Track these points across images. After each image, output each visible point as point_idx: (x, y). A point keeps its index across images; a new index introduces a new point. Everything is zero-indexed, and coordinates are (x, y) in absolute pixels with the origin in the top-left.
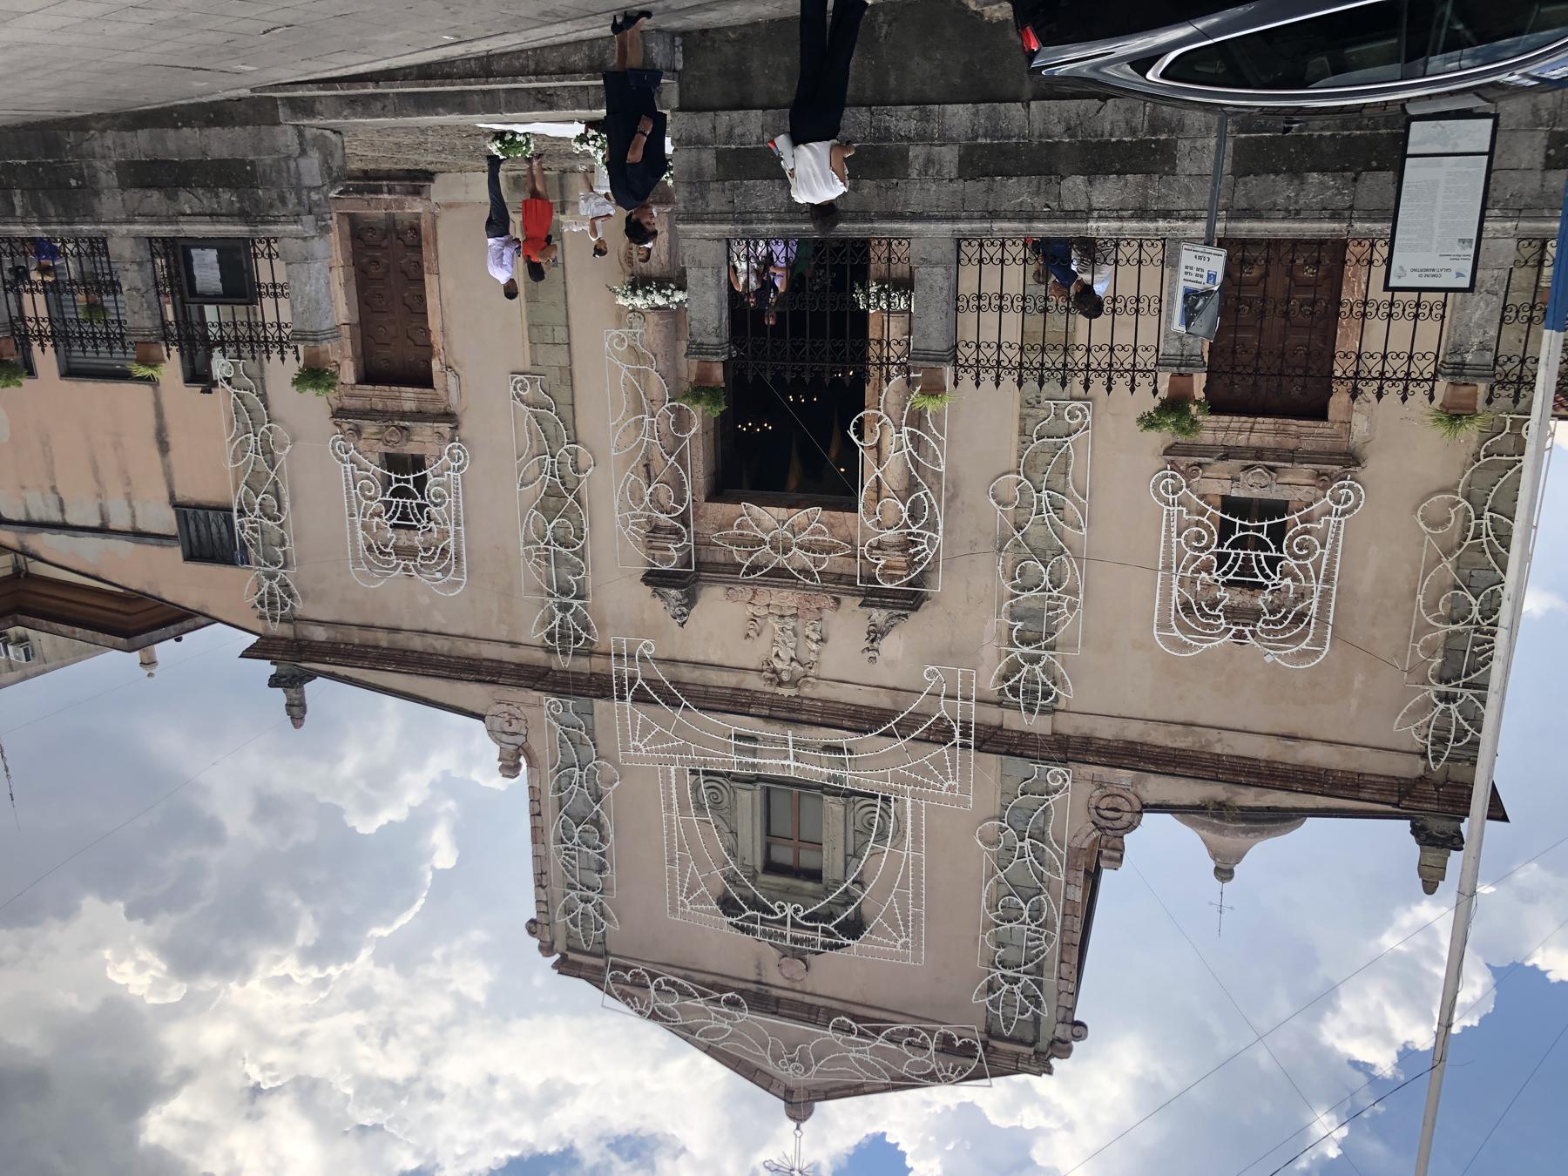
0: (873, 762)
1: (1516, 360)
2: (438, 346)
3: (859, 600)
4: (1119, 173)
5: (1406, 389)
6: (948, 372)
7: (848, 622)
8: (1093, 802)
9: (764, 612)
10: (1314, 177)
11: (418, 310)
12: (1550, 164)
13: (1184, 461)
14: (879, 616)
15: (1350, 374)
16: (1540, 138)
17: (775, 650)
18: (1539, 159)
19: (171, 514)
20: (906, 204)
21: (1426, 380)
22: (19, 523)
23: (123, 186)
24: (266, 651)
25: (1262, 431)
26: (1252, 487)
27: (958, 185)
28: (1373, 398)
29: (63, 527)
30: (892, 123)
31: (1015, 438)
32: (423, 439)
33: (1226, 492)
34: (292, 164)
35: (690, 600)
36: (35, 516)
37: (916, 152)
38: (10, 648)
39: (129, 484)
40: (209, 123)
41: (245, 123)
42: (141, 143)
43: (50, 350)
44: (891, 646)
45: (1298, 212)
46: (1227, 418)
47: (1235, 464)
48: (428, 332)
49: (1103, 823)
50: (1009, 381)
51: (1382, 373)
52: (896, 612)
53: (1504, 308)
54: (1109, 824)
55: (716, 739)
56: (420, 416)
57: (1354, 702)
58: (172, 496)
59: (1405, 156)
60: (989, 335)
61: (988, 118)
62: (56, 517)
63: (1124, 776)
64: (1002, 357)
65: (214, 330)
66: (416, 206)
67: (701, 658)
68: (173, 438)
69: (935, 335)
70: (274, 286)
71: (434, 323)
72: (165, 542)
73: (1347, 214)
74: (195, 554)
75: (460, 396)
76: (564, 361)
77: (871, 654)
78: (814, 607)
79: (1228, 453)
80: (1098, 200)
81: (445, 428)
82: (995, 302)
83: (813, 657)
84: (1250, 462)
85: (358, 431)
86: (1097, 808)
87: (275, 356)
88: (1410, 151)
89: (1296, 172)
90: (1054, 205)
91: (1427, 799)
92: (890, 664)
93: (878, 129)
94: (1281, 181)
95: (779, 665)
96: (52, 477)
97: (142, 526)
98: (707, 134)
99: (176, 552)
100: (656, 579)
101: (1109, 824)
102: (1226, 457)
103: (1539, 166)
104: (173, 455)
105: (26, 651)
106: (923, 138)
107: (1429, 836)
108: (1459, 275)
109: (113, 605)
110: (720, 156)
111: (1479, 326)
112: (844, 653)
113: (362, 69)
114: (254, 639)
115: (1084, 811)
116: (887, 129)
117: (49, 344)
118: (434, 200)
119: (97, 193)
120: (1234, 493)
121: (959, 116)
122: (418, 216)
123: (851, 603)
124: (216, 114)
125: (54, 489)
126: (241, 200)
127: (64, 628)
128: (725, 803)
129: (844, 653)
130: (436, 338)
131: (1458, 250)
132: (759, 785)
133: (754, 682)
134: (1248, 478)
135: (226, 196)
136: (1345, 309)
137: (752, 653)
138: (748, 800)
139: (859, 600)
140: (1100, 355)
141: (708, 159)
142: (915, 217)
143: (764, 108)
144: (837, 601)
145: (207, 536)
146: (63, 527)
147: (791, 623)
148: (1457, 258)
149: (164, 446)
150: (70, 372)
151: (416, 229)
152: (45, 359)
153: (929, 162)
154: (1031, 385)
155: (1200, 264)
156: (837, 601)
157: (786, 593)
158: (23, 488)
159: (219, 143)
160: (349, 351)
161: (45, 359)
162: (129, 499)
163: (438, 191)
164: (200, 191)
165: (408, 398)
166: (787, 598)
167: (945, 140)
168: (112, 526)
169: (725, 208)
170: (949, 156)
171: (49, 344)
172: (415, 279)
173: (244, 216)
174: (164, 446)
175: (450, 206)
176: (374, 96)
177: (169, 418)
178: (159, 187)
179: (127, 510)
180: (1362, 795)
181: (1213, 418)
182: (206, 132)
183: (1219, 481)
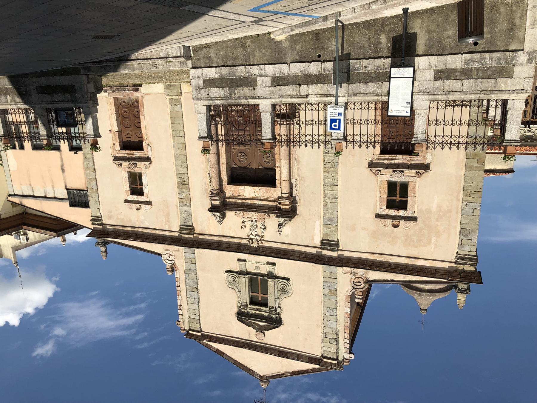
0: (283, 267)
1: (433, 136)
2: (145, 138)
3: (276, 215)
4: (316, 84)
5: (451, 146)
6: (344, 143)
7: (273, 221)
8: (352, 280)
9: (247, 220)
10: (370, 84)
11: (138, 127)
12: (435, 79)
13: (374, 169)
14: (282, 220)
15: (373, 141)
16: (432, 72)
17: (251, 232)
18: (432, 78)
19: (66, 192)
20: (257, 94)
21: (472, 144)
22: (237, 272)
23: (38, 94)
24: (94, 234)
25: (399, 159)
26: (398, 178)
27: (271, 88)
28: (433, 149)
29: (33, 197)
30: (251, 71)
31: (322, 163)
32: (141, 166)
33: (389, 179)
34: (85, 86)
35: (223, 216)
36: (25, 194)
37: (259, 79)
38: (21, 236)
39: (53, 183)
40: (62, 75)
41: (71, 74)
42: (44, 81)
43: (66, 142)
44: (286, 229)
45: (367, 94)
46: (387, 156)
47: (391, 170)
48: (142, 133)
49: (356, 287)
50: (462, 148)
51: (360, 141)
52: (287, 219)
53: (429, 121)
54: (357, 287)
55: (231, 260)
56: (140, 159)
57: (433, 246)
58: (66, 186)
59: (390, 78)
60: (302, 132)
61: (279, 69)
62: (31, 194)
63: (361, 271)
64: (452, 140)
65: (25, 135)
66: (136, 95)
67: (228, 235)
68: (66, 169)
69: (268, 132)
70: (82, 121)
71: (143, 130)
72: (64, 201)
73: (380, 94)
74: (73, 204)
75: (152, 153)
76: (183, 142)
77: (280, 232)
78: (262, 218)
79: (388, 166)
80: (311, 92)
81: (147, 163)
82: (314, 123)
83: (262, 234)
84: (395, 169)
85: (121, 165)
86: (353, 282)
87: (26, 140)
88: (392, 76)
89: (365, 82)
90: (298, 94)
91: (457, 277)
92: (287, 236)
93: (248, 72)
94: (361, 85)
95: (252, 237)
96: (29, 180)
97: (57, 196)
98: (201, 76)
99: (67, 204)
100: (213, 209)
101: (357, 287)
102: (387, 168)
103: (433, 80)
104: (66, 173)
105: (26, 237)
106: (260, 75)
107: (459, 290)
108: (407, 112)
109: (52, 222)
110: (204, 81)
111: (421, 126)
112: (272, 231)
113: (102, 59)
114: (91, 231)
115: (349, 283)
116: (250, 72)
117: (322, 145)
118: (142, 92)
119: (31, 96)
120: (391, 179)
121: (271, 70)
122: (138, 97)
123: (273, 216)
124: (65, 72)
125: (30, 185)
126: (71, 97)
127: (37, 230)
128: (237, 282)
129: (272, 231)
130: (144, 135)
131: (406, 105)
132: (247, 276)
133: (245, 242)
134: (395, 175)
135: (67, 95)
136: (380, 122)
137: (245, 233)
138: (244, 281)
139: (276, 215)
140: (315, 137)
141: (201, 82)
142: (260, 98)
143: (215, 67)
144: (269, 216)
145: (78, 199)
146: (33, 197)
147: (255, 223)
148: (406, 107)
149: (63, 170)
150: (35, 148)
151: (137, 101)
152: (27, 145)
153: (263, 82)
154: (471, 148)
155: (335, 111)
156: (269, 216)
157: (253, 213)
158: (21, 184)
159: (64, 80)
160: (118, 140)
161: (27, 145)
162: (53, 187)
163: (144, 89)
164: (60, 94)
165: (136, 154)
166: (253, 215)
167: (265, 76)
168: (48, 196)
169: (207, 96)
170: (268, 81)
171: (322, 145)
172: (138, 117)
173: (72, 101)
174: (63, 170)
175: (147, 94)
176: (108, 66)
177: (64, 162)
178: (49, 94)
179: (53, 191)
180: (436, 276)
181: (383, 155)
182: (61, 77)
183: (387, 175)
